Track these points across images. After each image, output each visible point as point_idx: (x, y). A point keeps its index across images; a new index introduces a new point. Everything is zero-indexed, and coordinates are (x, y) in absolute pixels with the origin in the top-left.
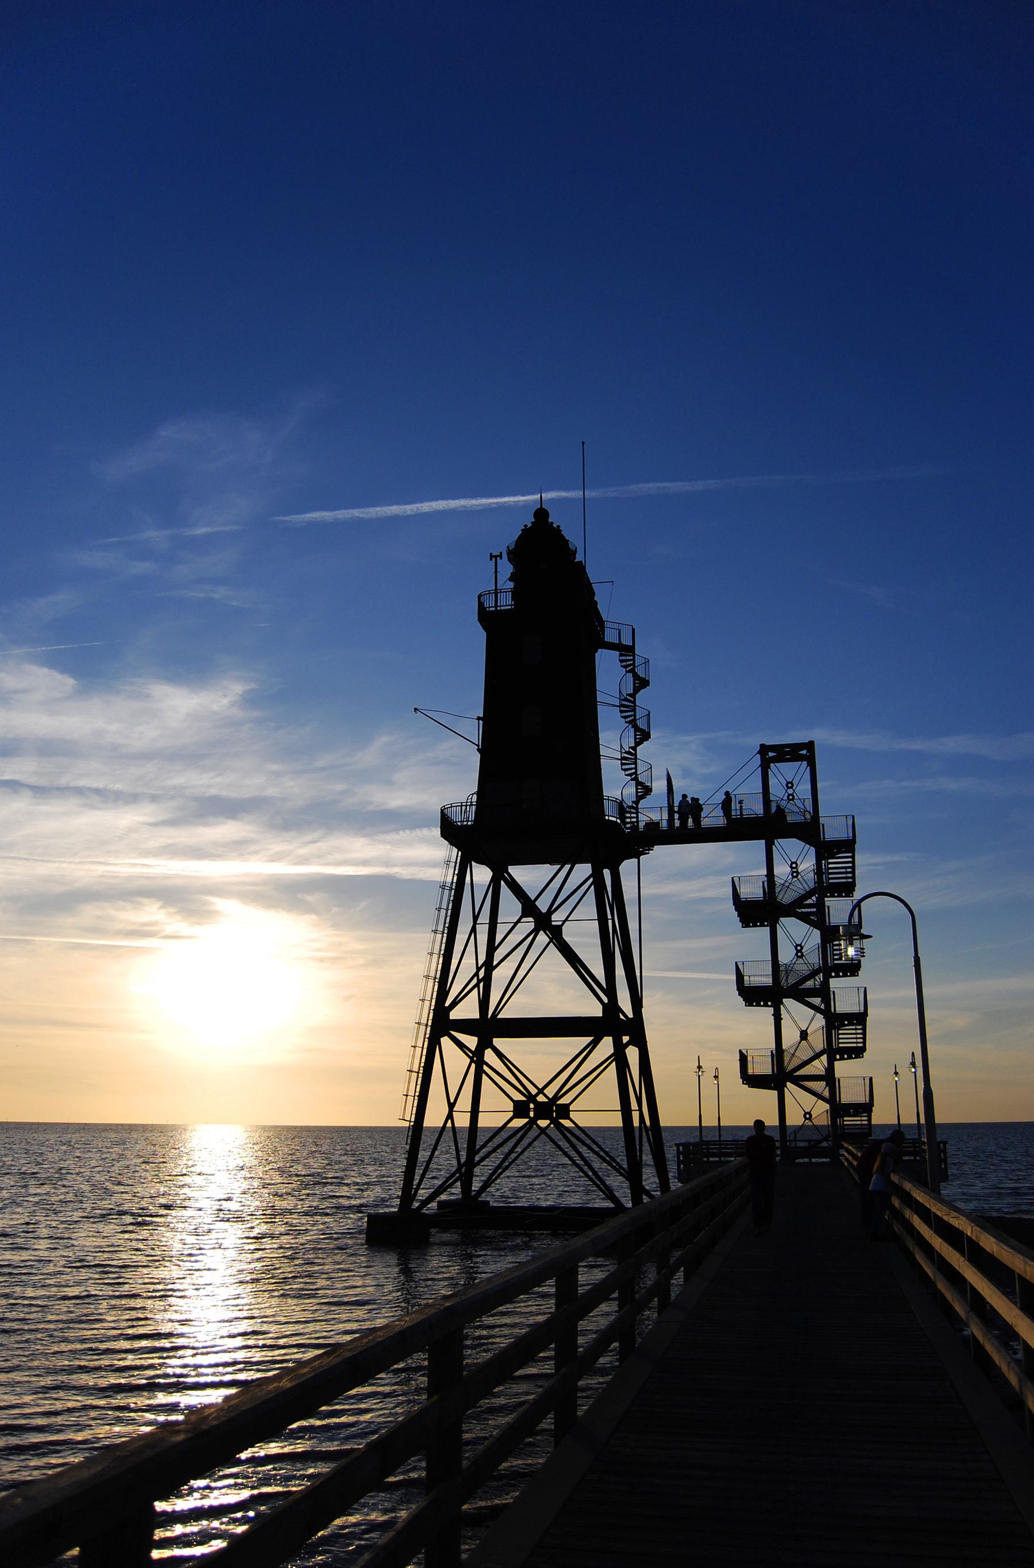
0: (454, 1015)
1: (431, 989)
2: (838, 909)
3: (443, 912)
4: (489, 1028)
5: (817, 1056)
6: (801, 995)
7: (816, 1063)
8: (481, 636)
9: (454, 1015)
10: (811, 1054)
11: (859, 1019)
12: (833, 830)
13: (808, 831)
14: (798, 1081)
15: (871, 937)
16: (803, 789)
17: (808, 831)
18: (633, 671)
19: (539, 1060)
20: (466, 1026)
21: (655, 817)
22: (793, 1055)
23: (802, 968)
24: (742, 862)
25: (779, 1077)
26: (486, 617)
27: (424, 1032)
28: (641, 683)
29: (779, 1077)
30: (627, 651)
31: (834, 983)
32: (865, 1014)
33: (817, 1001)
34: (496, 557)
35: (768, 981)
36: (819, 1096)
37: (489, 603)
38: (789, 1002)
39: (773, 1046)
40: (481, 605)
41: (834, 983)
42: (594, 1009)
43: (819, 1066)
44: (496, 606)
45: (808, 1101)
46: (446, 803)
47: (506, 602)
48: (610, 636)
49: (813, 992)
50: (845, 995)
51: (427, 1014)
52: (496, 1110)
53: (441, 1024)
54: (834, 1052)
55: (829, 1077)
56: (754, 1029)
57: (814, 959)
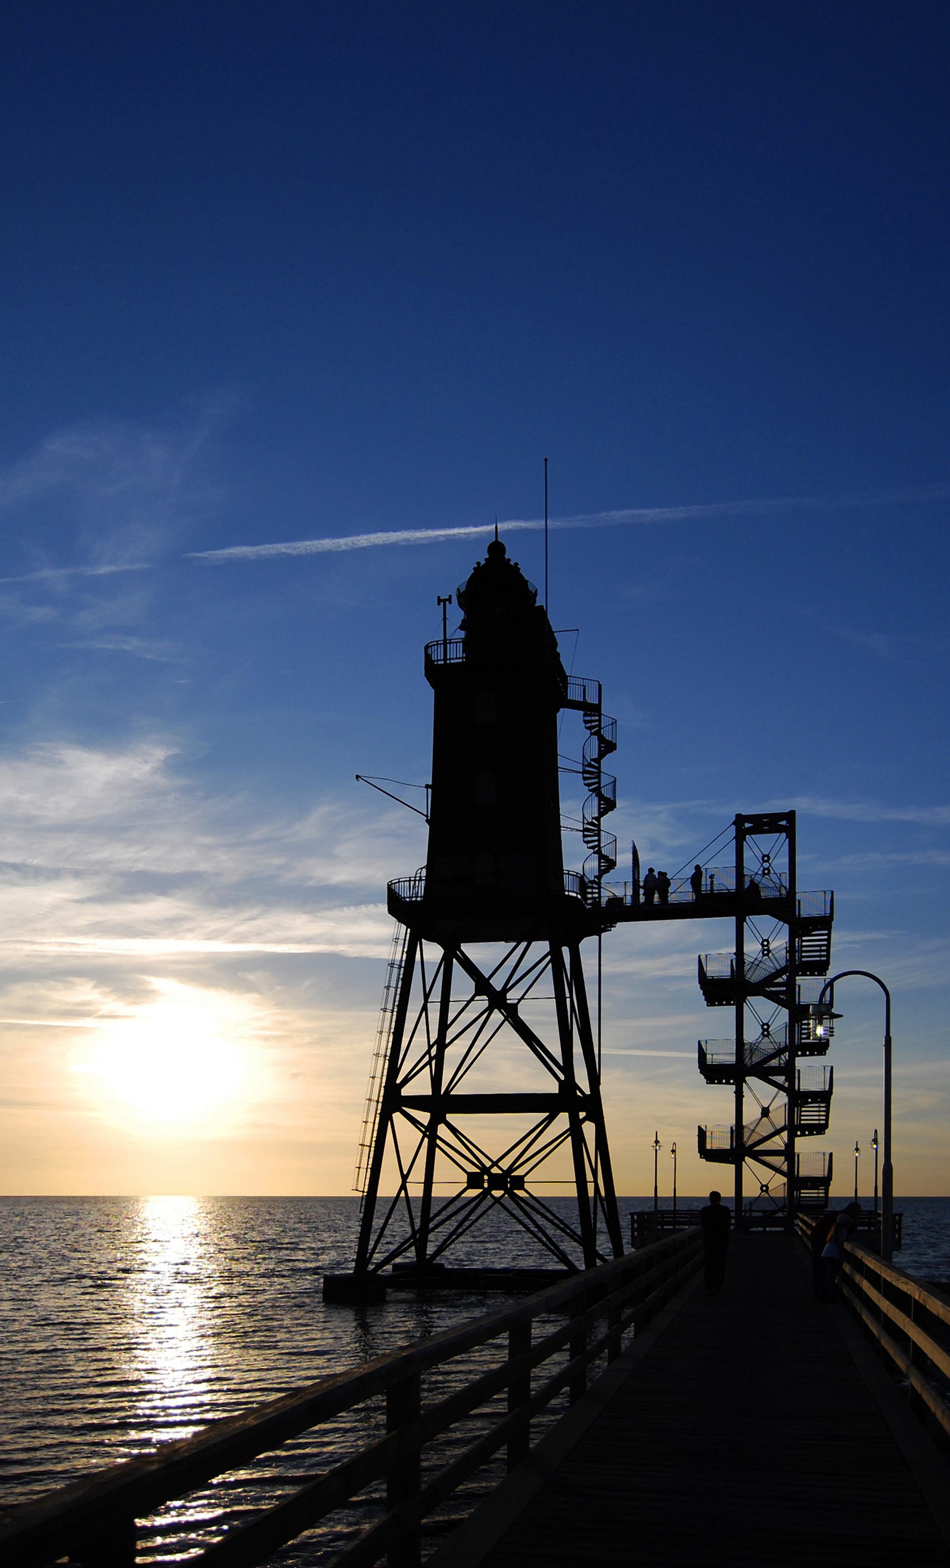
0: (405, 1092)
1: (382, 1066)
2: (809, 988)
3: (392, 990)
4: (441, 1104)
5: (778, 1132)
6: (764, 1074)
7: (776, 1139)
8: (427, 695)
9: (405, 1092)
10: (772, 1130)
11: (824, 1097)
12: (809, 907)
13: (783, 906)
14: (756, 1156)
15: (841, 1016)
16: (780, 863)
17: (783, 906)
18: (598, 733)
19: (493, 1135)
20: (418, 1102)
21: (619, 893)
22: (753, 1131)
23: (767, 1046)
24: (710, 941)
25: (738, 1151)
26: (434, 672)
27: (374, 1110)
28: (607, 747)
29: (738, 1151)
30: (592, 710)
31: (801, 1063)
32: (830, 1092)
33: (780, 1079)
34: (444, 601)
35: (732, 1059)
36: (778, 1170)
37: (437, 655)
38: (752, 1081)
39: (733, 1122)
40: (428, 657)
41: (801, 1063)
42: (552, 1087)
43: (779, 1142)
44: (445, 659)
45: (765, 1174)
46: (393, 878)
47: (456, 654)
48: (574, 694)
49: (777, 1071)
50: (810, 1073)
51: (377, 1091)
52: (450, 1181)
53: (393, 1100)
54: (794, 1128)
55: (789, 1152)
56: (715, 1107)
57: (780, 1037)
